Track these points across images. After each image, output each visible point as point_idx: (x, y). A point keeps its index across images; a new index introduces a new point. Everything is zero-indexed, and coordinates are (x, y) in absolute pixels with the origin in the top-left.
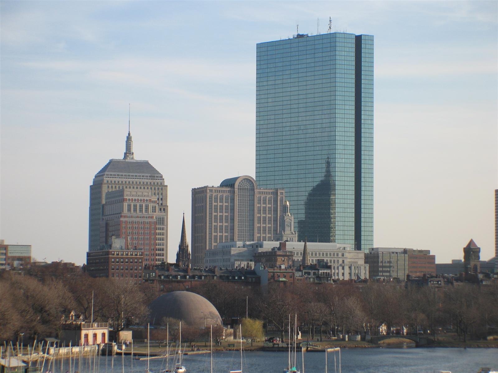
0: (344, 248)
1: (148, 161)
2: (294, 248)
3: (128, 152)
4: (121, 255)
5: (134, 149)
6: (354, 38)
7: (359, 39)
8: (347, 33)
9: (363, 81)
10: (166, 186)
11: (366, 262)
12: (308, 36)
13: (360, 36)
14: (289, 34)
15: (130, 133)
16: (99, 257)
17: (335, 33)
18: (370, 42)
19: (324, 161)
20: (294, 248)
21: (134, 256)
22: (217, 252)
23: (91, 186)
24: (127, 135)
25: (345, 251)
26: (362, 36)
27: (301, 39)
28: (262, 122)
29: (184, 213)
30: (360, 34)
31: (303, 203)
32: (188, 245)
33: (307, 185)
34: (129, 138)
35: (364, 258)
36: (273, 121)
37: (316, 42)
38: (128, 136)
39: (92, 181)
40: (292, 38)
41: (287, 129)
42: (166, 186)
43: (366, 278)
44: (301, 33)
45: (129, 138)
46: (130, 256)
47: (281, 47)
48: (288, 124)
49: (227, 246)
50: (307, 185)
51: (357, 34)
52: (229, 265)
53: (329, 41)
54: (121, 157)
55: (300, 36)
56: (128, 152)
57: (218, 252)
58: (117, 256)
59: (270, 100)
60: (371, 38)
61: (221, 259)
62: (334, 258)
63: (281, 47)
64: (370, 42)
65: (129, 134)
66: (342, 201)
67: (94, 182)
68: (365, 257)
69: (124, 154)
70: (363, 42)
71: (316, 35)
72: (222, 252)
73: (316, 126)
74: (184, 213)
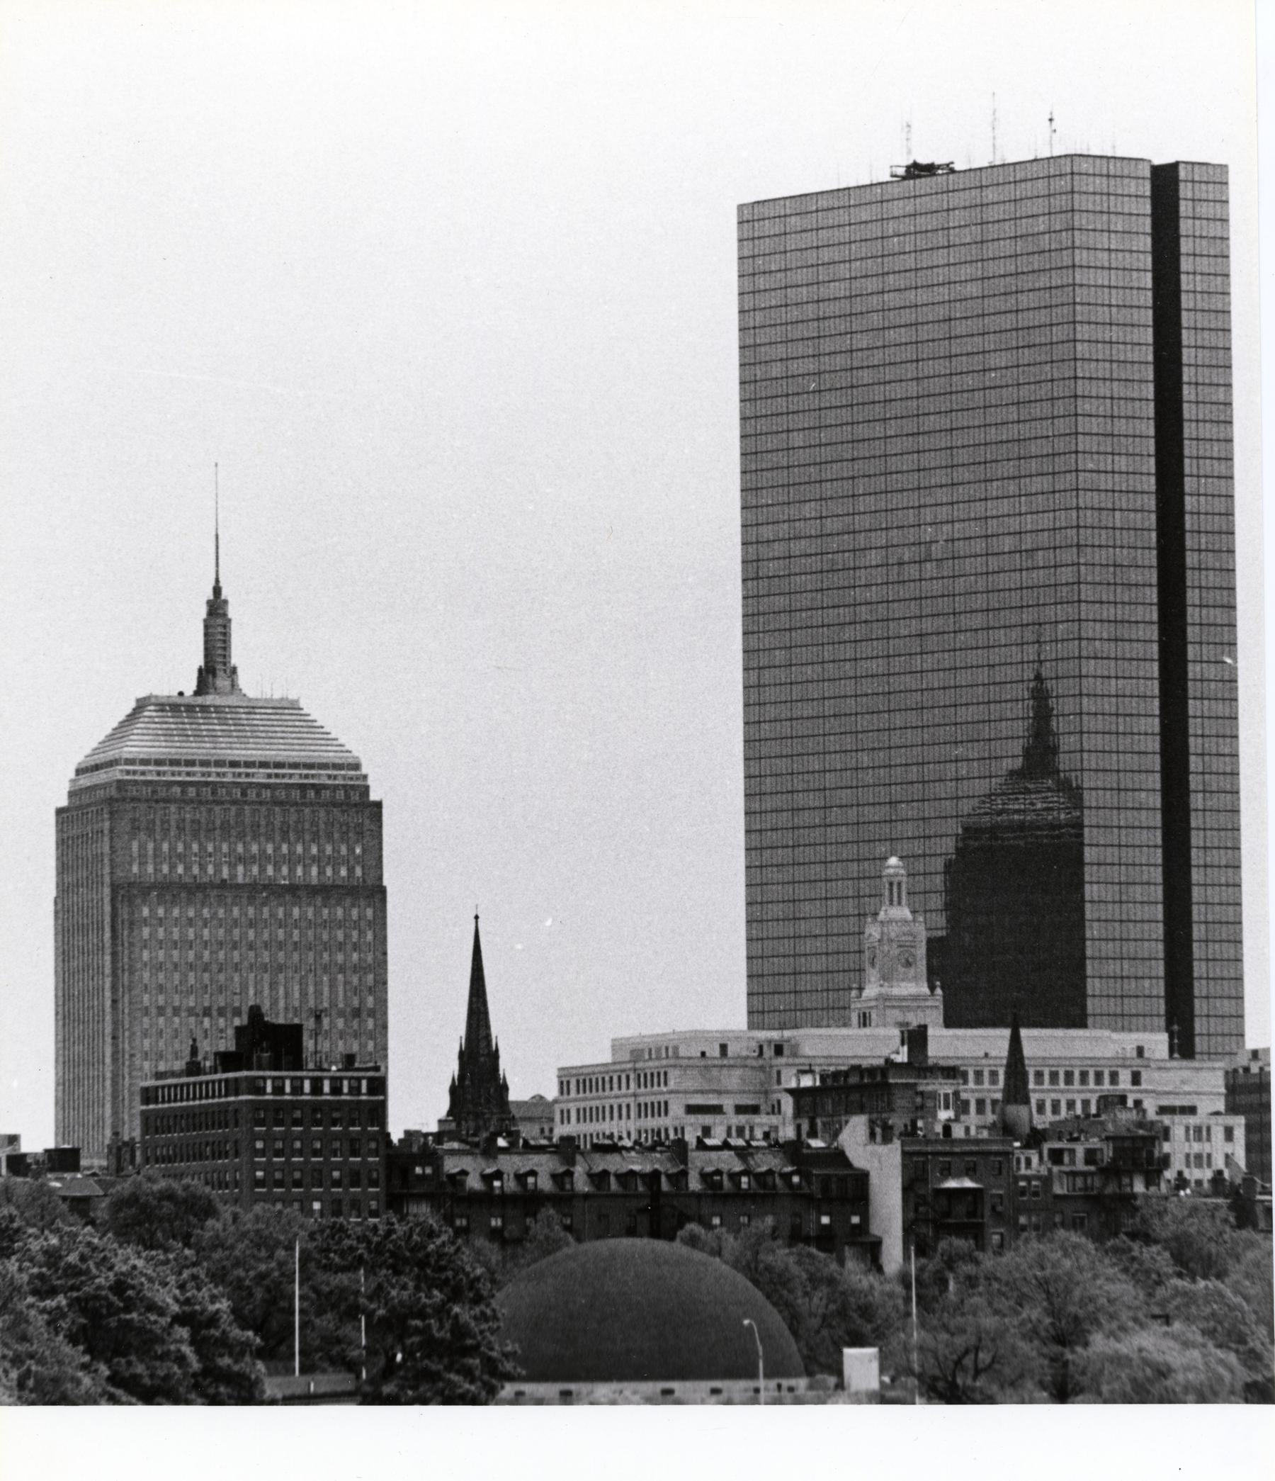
0: (1140, 1051)
1: (297, 701)
2: (703, 1054)
3: (216, 665)
4: (350, 1093)
5: (243, 651)
6: (1148, 174)
7: (1164, 180)
8: (1119, 154)
9: (1187, 355)
10: (378, 805)
11: (1232, 1109)
12: (953, 171)
13: (1174, 166)
14: (870, 161)
15: (221, 584)
16: (184, 1104)
17: (1066, 156)
18: (1211, 192)
19: (1022, 691)
20: (703, 1054)
21: (271, 1097)
22: (611, 1078)
23: (59, 812)
24: (211, 596)
25: (1145, 1063)
26: (1181, 167)
27: (924, 184)
28: (767, 532)
29: (477, 917)
30: (1171, 160)
31: (939, 864)
32: (497, 1050)
33: (965, 787)
34: (217, 609)
35: (1223, 1090)
36: (812, 528)
37: (1026, 189)
38: (211, 597)
39: (65, 788)
40: (888, 178)
41: (874, 557)
42: (378, 805)
43: (132, 1139)
44: (923, 160)
45: (217, 609)
46: (328, 1098)
47: (843, 217)
48: (880, 539)
49: (650, 1050)
50: (965, 787)
51: (1158, 160)
52: (562, 1122)
53: (1061, 182)
54: (181, 679)
55: (917, 171)
56: (216, 665)
57: (607, 1079)
58: (294, 1098)
59: (798, 439)
60: (1216, 176)
61: (628, 1106)
62: (1073, 1092)
63: (843, 217)
64: (1211, 192)
65: (217, 590)
66: (1111, 855)
67: (71, 794)
68: (1227, 1087)
69: (195, 675)
70: (1185, 191)
71: (986, 165)
72: (632, 1076)
73: (995, 545)
74: (477, 917)
